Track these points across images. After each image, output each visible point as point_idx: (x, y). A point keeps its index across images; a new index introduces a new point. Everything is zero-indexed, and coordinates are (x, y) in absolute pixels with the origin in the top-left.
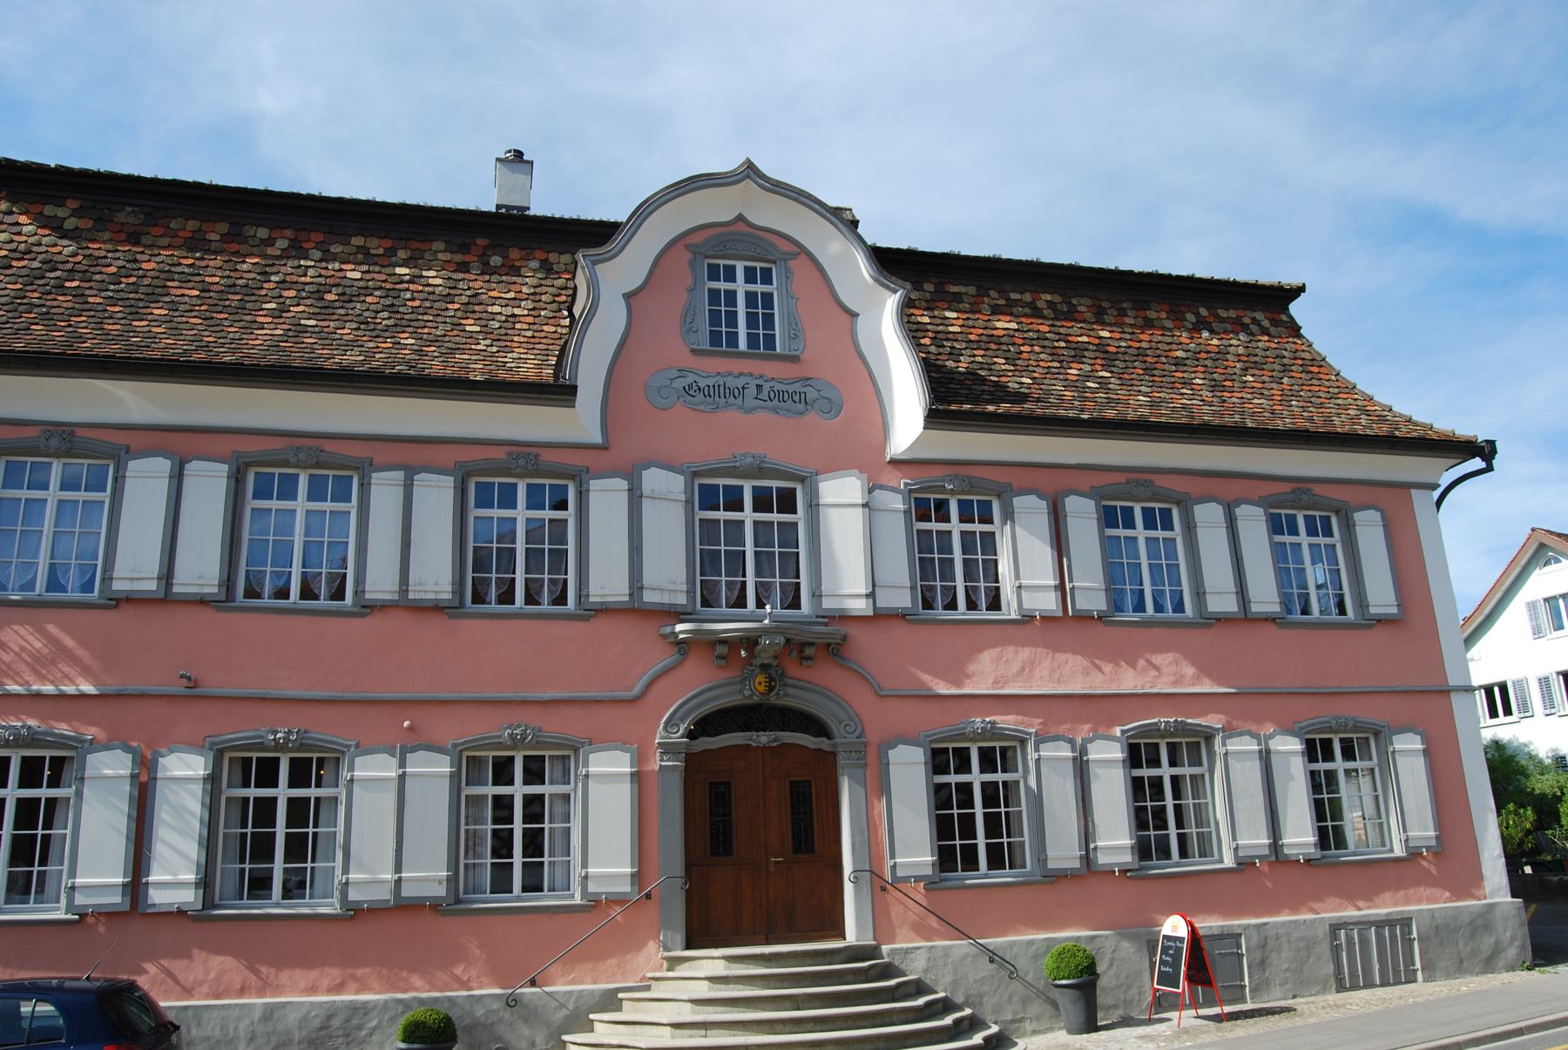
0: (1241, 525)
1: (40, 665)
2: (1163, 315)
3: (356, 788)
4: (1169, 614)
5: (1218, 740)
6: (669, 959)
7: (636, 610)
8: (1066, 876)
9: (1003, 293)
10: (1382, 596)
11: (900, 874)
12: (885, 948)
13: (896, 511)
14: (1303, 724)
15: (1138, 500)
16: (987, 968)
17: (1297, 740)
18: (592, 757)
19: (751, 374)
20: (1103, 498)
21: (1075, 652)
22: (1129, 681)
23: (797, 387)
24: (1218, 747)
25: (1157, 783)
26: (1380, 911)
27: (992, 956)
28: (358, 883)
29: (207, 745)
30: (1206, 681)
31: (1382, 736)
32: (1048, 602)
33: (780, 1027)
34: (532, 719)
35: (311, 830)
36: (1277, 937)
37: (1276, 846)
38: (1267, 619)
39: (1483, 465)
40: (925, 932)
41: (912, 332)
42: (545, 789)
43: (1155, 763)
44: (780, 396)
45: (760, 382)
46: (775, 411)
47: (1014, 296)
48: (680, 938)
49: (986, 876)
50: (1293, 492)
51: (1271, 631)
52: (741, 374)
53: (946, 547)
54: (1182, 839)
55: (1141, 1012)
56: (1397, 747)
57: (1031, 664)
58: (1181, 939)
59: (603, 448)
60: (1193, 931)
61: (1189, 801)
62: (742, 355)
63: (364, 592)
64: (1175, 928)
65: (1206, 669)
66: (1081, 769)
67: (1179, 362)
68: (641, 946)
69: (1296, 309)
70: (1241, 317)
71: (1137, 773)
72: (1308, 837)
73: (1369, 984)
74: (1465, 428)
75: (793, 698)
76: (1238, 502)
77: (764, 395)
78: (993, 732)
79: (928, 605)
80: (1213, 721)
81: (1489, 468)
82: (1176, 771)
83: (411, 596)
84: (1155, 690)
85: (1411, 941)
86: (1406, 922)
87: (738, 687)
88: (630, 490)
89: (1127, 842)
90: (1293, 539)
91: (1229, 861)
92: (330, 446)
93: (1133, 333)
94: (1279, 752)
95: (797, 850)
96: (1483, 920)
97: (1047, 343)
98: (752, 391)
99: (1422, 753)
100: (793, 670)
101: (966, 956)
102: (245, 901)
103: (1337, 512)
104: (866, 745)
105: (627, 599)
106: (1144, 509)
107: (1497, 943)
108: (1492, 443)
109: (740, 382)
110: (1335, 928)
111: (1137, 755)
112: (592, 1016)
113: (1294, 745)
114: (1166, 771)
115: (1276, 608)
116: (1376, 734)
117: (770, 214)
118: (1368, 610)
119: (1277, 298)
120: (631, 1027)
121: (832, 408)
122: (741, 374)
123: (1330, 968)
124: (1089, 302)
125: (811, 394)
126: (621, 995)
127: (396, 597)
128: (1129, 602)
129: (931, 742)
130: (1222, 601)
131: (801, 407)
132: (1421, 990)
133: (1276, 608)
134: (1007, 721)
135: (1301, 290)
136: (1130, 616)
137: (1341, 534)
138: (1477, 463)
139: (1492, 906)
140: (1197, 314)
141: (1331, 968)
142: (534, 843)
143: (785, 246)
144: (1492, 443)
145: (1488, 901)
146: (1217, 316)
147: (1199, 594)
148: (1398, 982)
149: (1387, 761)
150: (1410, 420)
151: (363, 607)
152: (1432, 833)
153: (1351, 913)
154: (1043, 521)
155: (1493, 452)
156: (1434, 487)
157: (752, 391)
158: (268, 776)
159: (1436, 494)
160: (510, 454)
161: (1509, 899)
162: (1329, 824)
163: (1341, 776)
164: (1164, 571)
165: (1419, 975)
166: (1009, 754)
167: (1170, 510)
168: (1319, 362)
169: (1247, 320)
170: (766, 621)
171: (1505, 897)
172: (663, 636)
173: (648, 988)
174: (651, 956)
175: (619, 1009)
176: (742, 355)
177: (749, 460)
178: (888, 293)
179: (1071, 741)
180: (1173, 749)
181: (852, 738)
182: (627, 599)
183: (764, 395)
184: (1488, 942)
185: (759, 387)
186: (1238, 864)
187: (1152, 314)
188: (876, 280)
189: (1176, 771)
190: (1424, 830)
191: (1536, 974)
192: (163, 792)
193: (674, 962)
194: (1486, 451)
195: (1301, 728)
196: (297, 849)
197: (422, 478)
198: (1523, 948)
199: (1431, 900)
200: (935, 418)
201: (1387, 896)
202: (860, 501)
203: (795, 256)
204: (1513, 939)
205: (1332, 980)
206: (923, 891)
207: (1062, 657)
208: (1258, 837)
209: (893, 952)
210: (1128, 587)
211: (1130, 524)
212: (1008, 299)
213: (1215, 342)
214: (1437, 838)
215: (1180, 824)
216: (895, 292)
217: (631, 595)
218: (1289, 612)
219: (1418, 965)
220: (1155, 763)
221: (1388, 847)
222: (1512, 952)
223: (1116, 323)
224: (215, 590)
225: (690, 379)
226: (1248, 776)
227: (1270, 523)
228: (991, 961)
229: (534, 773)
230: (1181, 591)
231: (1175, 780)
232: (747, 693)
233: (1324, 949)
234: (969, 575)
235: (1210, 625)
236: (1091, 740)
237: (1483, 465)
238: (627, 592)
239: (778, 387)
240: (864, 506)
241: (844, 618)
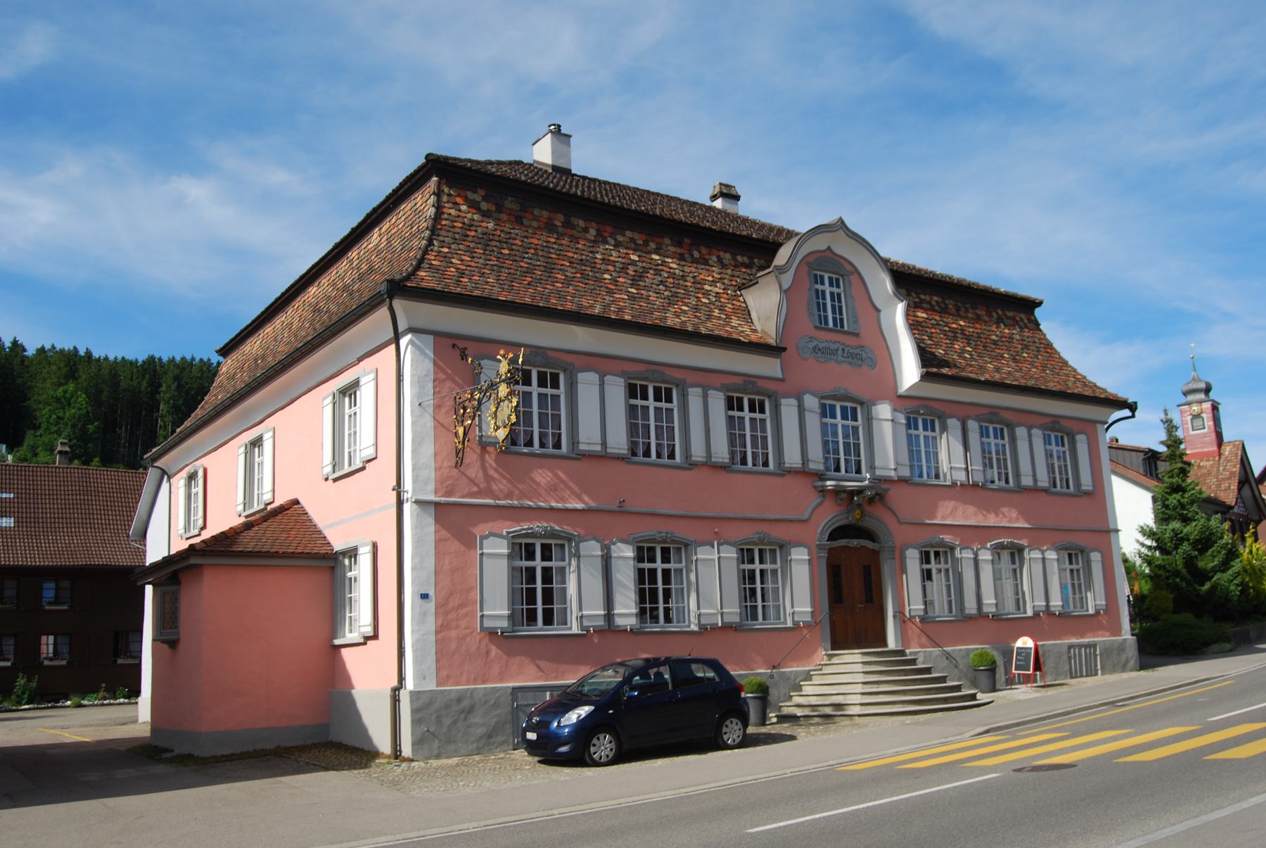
0: (1034, 439)
1: (553, 489)
2: (984, 313)
3: (484, 558)
4: (665, 460)
5: (957, 551)
6: (828, 655)
7: (803, 473)
8: (732, 627)
9: (751, 258)
10: (1086, 482)
11: (912, 614)
12: (908, 651)
13: (902, 424)
14: (635, 536)
15: (651, 381)
16: (945, 663)
17: (631, 547)
18: (792, 550)
19: (839, 342)
20: (822, 398)
21: (971, 504)
22: (992, 520)
23: (857, 351)
24: (1026, 555)
25: (653, 572)
26: (1086, 640)
27: (948, 656)
28: (728, 613)
29: (631, 539)
30: (1021, 520)
31: (689, 547)
32: (961, 477)
33: (919, 682)
34: (765, 528)
35: (524, 586)
36: (1049, 651)
37: (1048, 606)
38: (721, 467)
39: (1130, 414)
40: (922, 646)
41: (914, 326)
42: (672, 566)
43: (652, 560)
44: (851, 355)
45: (843, 347)
46: (850, 364)
47: (922, 297)
48: (829, 646)
49: (541, 630)
50: (990, 413)
51: (1043, 495)
52: (836, 342)
53: (646, 416)
54: (667, 610)
55: (1002, 685)
56: (794, 557)
57: (954, 509)
58: (1030, 649)
59: (782, 380)
60: (1036, 647)
61: (769, 585)
62: (830, 330)
63: (691, 456)
64: (1025, 643)
65: (1024, 515)
66: (976, 562)
67: (995, 343)
68: (815, 651)
69: (1037, 312)
70: (521, 210)
71: (743, 566)
72: (806, 607)
73: (1081, 676)
74: (1122, 394)
75: (868, 523)
76: (969, 417)
77: (845, 355)
78: (942, 544)
79: (514, 443)
80: (1024, 542)
81: (1133, 416)
82: (763, 566)
83: (713, 460)
84: (1001, 525)
85: (1096, 655)
86: (1094, 646)
87: (846, 515)
88: (799, 406)
89: (634, 611)
90: (740, 414)
91: (1030, 613)
92: (668, 371)
93: (627, 253)
94: (1049, 559)
95: (867, 602)
96: (1122, 647)
97: (940, 327)
98: (840, 352)
99: (807, 562)
100: (867, 508)
101: (937, 656)
102: (525, 627)
103: (677, 386)
104: (895, 547)
105: (800, 466)
106: (841, 407)
107: (1127, 658)
108: (1136, 403)
109: (834, 346)
110: (1071, 647)
111: (643, 554)
112: (802, 683)
113: (629, 552)
114: (757, 566)
115: (822, 467)
116: (781, 547)
117: (844, 249)
118: (578, 446)
119: (1029, 305)
120: (832, 687)
121: (873, 363)
122: (836, 342)
123: (1067, 667)
124: (953, 303)
125: (864, 356)
126: (812, 673)
127: (704, 460)
128: (522, 440)
129: (637, 542)
130: (1027, 481)
131: (860, 362)
132: (1099, 679)
133: (822, 467)
134: (948, 538)
135: (1040, 304)
136: (641, 458)
137: (771, 413)
138: (1127, 413)
139: (1125, 640)
140: (997, 313)
141: (1068, 667)
142: (548, 597)
143: (848, 267)
144: (1136, 403)
145: (1123, 637)
146: (1005, 315)
147: (1017, 475)
148: (1091, 675)
149: (786, 562)
150: (1096, 386)
151: (690, 464)
152: (1104, 603)
153: (1074, 641)
154: (959, 432)
155: (1136, 408)
156: (1106, 423)
157: (840, 352)
158: (530, 556)
159: (1106, 426)
160: (745, 381)
161: (1130, 637)
162: (648, 605)
163: (934, 572)
164: (665, 432)
165: (1099, 672)
166: (764, 552)
167: (558, 374)
168: (1049, 346)
169: (1018, 319)
170: (867, 482)
171: (1129, 637)
172: (815, 487)
173: (821, 670)
174: (821, 654)
175: (811, 680)
176: (830, 330)
177: (843, 392)
178: (898, 301)
179: (973, 549)
180: (937, 554)
181: (890, 544)
182: (800, 466)
183: (845, 355)
184: (1124, 657)
185: (843, 349)
186: (700, 629)
187: (979, 312)
188: (894, 294)
189: (763, 566)
190: (1102, 602)
191: (1142, 673)
192: (615, 564)
193: (830, 657)
194: (1133, 407)
195: (634, 538)
196: (531, 597)
197: (608, 378)
198: (1136, 661)
199: (1103, 636)
200: (926, 377)
201: (1089, 634)
202: (891, 418)
203: (852, 273)
204: (1133, 656)
205: (1068, 673)
206: (919, 624)
207: (967, 506)
208: (1041, 602)
209: (911, 653)
210: (641, 440)
211: (645, 397)
212: (920, 298)
213: (1007, 331)
214: (1106, 605)
215: (666, 601)
216: (902, 301)
217: (803, 464)
218: (634, 454)
219: (1099, 667)
220: (652, 560)
221: (782, 619)
222: (1132, 663)
223: (539, 227)
224: (626, 452)
225: (815, 343)
226: (1038, 568)
227: (627, 389)
228: (947, 658)
229: (546, 556)
230: (767, 453)
231: (762, 571)
232: (850, 519)
233: (1065, 657)
234: (754, 445)
235: (1081, 496)
236: (980, 549)
237: (1130, 414)
238: (801, 462)
239: (851, 351)
240: (892, 420)
241: (888, 480)
